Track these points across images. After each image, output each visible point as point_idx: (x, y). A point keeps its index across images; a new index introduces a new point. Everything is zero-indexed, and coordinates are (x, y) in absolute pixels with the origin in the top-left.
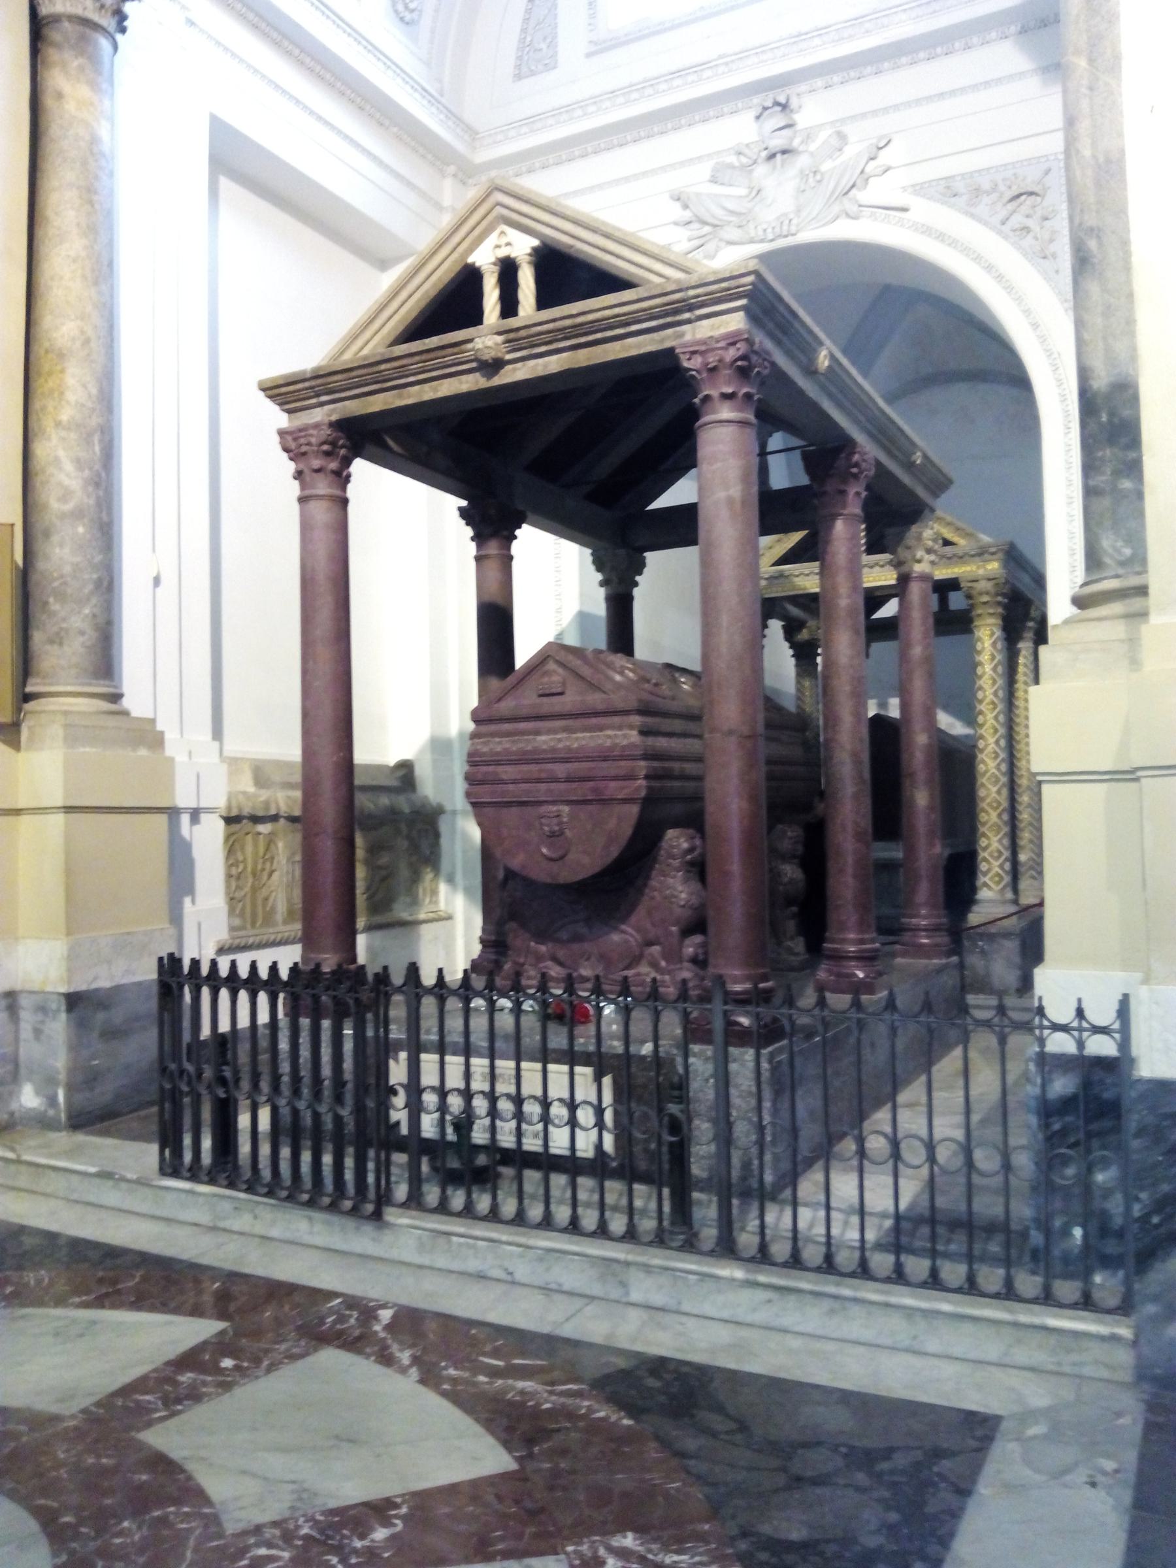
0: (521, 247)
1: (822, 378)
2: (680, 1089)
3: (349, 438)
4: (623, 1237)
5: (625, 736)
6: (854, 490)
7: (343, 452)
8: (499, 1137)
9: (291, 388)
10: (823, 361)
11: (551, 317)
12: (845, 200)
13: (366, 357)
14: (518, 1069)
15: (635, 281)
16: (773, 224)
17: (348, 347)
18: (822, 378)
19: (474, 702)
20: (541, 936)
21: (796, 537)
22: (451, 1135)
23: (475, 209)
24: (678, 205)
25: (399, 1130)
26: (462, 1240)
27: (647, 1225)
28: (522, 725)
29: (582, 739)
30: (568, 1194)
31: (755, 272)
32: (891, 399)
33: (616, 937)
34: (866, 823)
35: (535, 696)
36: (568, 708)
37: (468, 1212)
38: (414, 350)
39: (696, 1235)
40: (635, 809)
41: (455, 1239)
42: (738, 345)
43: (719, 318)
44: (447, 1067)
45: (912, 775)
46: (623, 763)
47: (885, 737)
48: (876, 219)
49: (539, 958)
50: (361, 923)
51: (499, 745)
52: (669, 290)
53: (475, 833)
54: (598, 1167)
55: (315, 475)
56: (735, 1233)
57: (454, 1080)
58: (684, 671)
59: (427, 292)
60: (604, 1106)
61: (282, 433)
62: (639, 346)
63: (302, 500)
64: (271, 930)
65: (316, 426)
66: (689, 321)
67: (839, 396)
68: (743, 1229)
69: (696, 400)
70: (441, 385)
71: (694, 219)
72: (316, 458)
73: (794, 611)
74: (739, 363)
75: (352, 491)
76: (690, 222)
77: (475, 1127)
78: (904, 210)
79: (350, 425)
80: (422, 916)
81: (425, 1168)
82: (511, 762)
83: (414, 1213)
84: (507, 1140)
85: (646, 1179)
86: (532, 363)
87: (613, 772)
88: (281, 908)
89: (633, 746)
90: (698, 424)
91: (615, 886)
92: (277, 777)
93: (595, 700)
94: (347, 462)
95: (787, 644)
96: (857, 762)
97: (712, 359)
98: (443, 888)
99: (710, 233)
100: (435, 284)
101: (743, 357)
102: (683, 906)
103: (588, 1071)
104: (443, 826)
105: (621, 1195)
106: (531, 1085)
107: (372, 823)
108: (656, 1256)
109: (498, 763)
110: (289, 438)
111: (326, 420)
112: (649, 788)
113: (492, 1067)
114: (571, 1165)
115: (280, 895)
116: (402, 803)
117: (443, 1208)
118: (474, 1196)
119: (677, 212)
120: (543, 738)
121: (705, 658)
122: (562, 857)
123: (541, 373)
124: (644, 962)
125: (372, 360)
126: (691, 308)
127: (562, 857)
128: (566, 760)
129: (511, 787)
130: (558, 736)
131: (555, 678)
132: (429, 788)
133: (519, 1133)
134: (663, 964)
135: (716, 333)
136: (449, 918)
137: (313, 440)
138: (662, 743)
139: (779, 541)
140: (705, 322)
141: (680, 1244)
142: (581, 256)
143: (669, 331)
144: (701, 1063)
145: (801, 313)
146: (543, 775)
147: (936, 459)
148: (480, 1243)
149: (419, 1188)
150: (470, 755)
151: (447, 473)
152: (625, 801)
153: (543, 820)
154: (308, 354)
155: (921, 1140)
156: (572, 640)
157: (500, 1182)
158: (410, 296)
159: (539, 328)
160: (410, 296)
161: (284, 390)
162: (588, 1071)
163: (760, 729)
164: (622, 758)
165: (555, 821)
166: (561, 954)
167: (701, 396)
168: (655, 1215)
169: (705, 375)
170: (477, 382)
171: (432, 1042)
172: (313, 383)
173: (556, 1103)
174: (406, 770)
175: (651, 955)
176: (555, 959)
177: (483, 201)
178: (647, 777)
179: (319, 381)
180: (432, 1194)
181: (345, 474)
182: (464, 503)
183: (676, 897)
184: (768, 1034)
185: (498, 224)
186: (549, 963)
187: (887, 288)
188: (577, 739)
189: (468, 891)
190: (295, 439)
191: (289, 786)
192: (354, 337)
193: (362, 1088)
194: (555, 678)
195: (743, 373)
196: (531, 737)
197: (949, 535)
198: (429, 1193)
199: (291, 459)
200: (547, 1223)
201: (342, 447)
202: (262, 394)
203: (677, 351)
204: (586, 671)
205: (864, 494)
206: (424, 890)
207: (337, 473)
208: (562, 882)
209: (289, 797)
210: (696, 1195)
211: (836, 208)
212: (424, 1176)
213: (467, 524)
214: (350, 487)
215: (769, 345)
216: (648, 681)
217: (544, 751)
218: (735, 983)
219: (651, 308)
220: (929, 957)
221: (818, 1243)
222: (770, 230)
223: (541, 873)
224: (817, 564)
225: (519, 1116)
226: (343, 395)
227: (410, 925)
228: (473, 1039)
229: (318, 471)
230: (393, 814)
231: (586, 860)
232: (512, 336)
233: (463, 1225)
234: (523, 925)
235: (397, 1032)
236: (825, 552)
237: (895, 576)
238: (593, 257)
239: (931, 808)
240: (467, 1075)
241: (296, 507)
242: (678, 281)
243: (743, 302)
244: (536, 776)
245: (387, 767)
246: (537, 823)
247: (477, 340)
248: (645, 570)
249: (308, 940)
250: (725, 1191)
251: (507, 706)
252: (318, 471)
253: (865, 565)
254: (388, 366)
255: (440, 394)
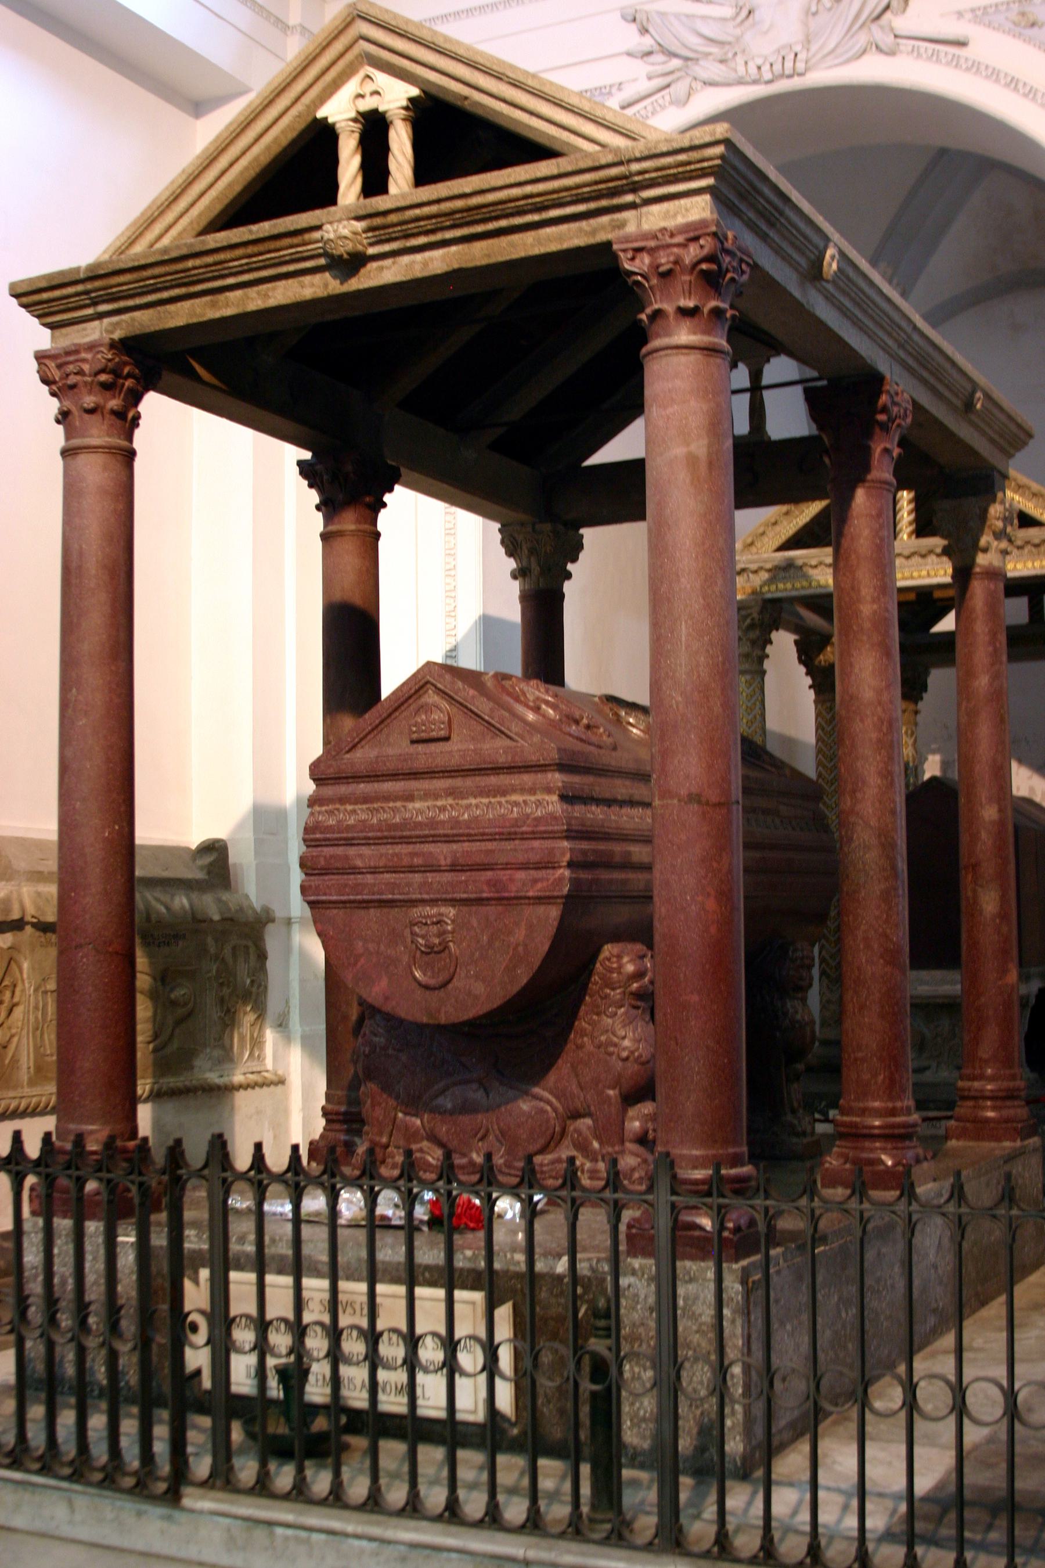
0: (394, 96)
1: (830, 287)
2: (608, 1318)
3: (137, 364)
4: (523, 1526)
5: (539, 804)
6: (882, 446)
7: (129, 383)
8: (344, 1392)
9: (57, 293)
10: (831, 265)
11: (434, 197)
12: (874, 28)
13: (165, 250)
14: (372, 1294)
15: (557, 147)
16: (772, 60)
17: (141, 235)
18: (830, 287)
19: (316, 749)
20: (413, 1104)
21: (813, 509)
22: (275, 1390)
23: (329, 44)
24: (633, 28)
25: (200, 1383)
26: (290, 1532)
27: (558, 1512)
28: (388, 786)
29: (476, 808)
30: (445, 1473)
31: (727, 142)
32: (935, 318)
33: (525, 1106)
34: (902, 936)
35: (406, 742)
36: (455, 761)
37: (299, 1493)
38: (236, 240)
39: (628, 1524)
40: (554, 913)
41: (279, 1531)
42: (702, 242)
43: (676, 202)
44: (268, 1291)
45: (975, 867)
46: (536, 844)
47: (934, 812)
48: (919, 56)
49: (412, 1136)
50: (144, 1086)
51: (354, 815)
52: (603, 162)
53: (316, 951)
54: (491, 1434)
55: (86, 416)
56: (683, 1520)
57: (280, 1305)
58: (633, 707)
59: (256, 159)
60: (497, 1339)
61: (40, 357)
62: (560, 238)
63: (66, 453)
64: (11, 1094)
65: (91, 347)
66: (633, 206)
67: (857, 312)
68: (698, 1516)
69: (643, 317)
70: (274, 289)
71: (656, 48)
72: (90, 392)
73: (812, 619)
74: (704, 266)
75: (140, 439)
76: (649, 53)
77: (311, 1378)
78: (961, 44)
79: (134, 345)
80: (238, 1078)
81: (237, 1434)
82: (368, 842)
83: (220, 1495)
84: (357, 1398)
85: (555, 1452)
86: (406, 259)
87: (521, 858)
88: (26, 1061)
89: (553, 817)
90: (644, 351)
91: (529, 1028)
92: (21, 864)
93: (496, 749)
94: (136, 398)
95: (802, 670)
96: (887, 846)
97: (665, 260)
98: (270, 1036)
99: (679, 70)
100: (268, 148)
101: (710, 258)
102: (627, 1059)
103: (478, 1297)
104: (272, 943)
105: (522, 1474)
106: (392, 1314)
107: (164, 934)
108: (569, 1552)
109: (349, 842)
110: (52, 365)
111: (106, 338)
112: (575, 883)
113: (334, 1290)
114: (450, 1432)
115: (25, 1041)
116: (210, 905)
117: (262, 1488)
118: (309, 1473)
119: (631, 38)
120: (418, 805)
121: (655, 687)
122: (444, 985)
123: (419, 274)
124: (567, 1141)
125: (174, 254)
126: (635, 188)
127: (444, 985)
128: (449, 839)
129: (369, 878)
130: (439, 803)
131: (436, 716)
132: (251, 888)
133: (374, 1387)
134: (596, 1145)
135: (670, 224)
136: (281, 1082)
137: (86, 367)
138: (596, 814)
139: (787, 513)
140: (655, 208)
141: (604, 1535)
142: (480, 112)
143: (605, 219)
144: (638, 1283)
145: (795, 196)
146: (416, 861)
147: (1006, 402)
148: (316, 1537)
149: (229, 1459)
150: (307, 830)
151: (281, 411)
152: (539, 900)
153: (416, 929)
154: (82, 242)
155: (947, 1382)
156: (470, 660)
157: (344, 1456)
158: (231, 165)
159: (417, 212)
160: (231, 165)
161: (45, 296)
162: (478, 1297)
163: (736, 792)
164: (534, 836)
165: (434, 929)
166: (442, 1130)
167: (648, 311)
168: (568, 1498)
169: (654, 281)
170: (326, 285)
171: (247, 1255)
172: (89, 286)
173: (429, 1340)
174: (215, 851)
175: (578, 1131)
176: (434, 1139)
177: (341, 32)
178: (570, 865)
179: (98, 284)
180: (247, 1469)
181: (131, 415)
182: (307, 455)
183: (615, 1045)
184: (740, 1243)
185: (361, 64)
186: (425, 1144)
187: (943, 152)
188: (468, 807)
189: (307, 1043)
190: (59, 367)
191: (37, 876)
192: (149, 221)
193: (146, 1317)
194: (436, 716)
195: (711, 279)
196: (398, 804)
197: (1031, 508)
198: (242, 1469)
199: (53, 394)
200: (413, 1508)
201: (129, 376)
202: (14, 301)
203: (615, 247)
204: (483, 706)
205: (896, 452)
206: (242, 1039)
207: (120, 415)
208: (443, 1020)
209: (39, 894)
210: (626, 1473)
211: (862, 39)
212: (235, 1446)
213: (311, 486)
214: (138, 434)
215: (749, 240)
216: (577, 722)
217: (419, 825)
218: (695, 1167)
219: (578, 187)
220: (999, 1139)
221: (802, 1533)
222: (766, 68)
223: (412, 1008)
224: (829, 550)
225: (374, 1360)
226: (130, 303)
227: (223, 1092)
228: (306, 1250)
229: (91, 411)
230: (197, 922)
231: (479, 988)
232: (378, 221)
233: (291, 1511)
234: (387, 1088)
235: (194, 1241)
236: (840, 534)
237: (950, 571)
238: (500, 114)
239: (1003, 916)
240: (299, 1304)
241: (59, 462)
242: (617, 150)
243: (710, 181)
244: (406, 861)
245: (187, 849)
246: (407, 932)
247: (327, 227)
248: (582, 556)
249: (64, 1107)
250: (667, 1464)
251: (363, 756)
252: (91, 411)
253: (899, 555)
254: (198, 262)
255: (272, 302)
